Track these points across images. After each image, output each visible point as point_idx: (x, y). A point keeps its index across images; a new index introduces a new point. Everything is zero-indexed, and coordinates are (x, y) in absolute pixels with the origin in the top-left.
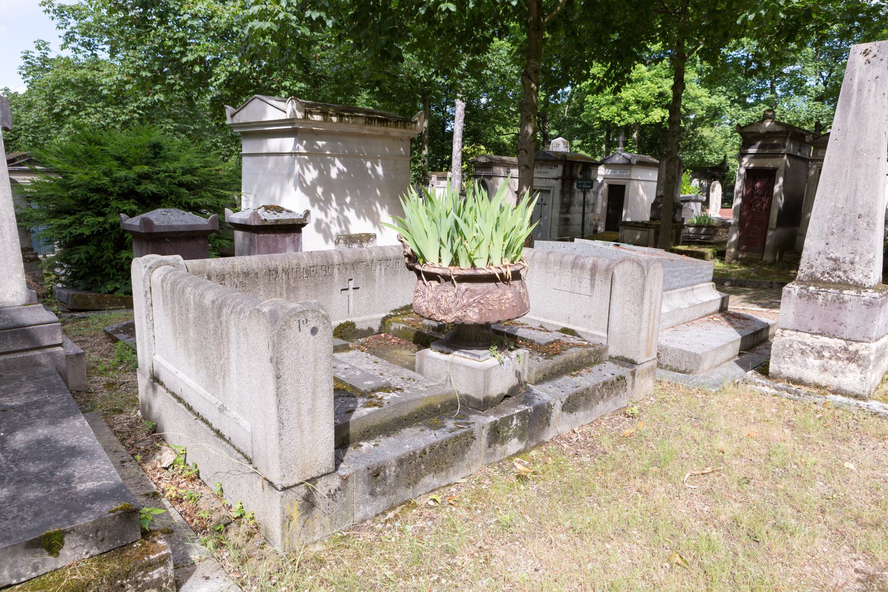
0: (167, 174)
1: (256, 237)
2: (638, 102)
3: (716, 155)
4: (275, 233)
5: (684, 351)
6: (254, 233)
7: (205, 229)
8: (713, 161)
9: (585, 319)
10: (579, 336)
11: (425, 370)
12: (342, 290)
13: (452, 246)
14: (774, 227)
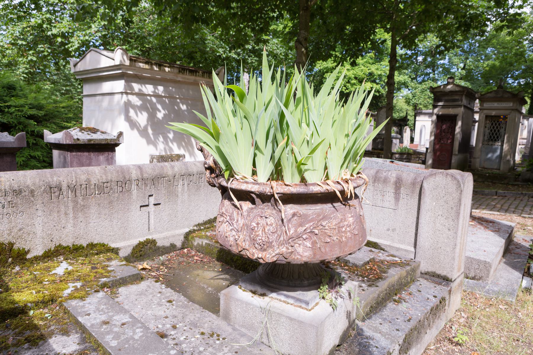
0: (17, 109)
1: (69, 155)
2: (356, 78)
3: (398, 114)
4: (88, 151)
5: (473, 258)
6: (68, 151)
7: (10, 146)
8: (396, 117)
9: (389, 232)
10: (383, 250)
11: (232, 316)
12: (141, 206)
13: (274, 152)
14: (457, 153)
